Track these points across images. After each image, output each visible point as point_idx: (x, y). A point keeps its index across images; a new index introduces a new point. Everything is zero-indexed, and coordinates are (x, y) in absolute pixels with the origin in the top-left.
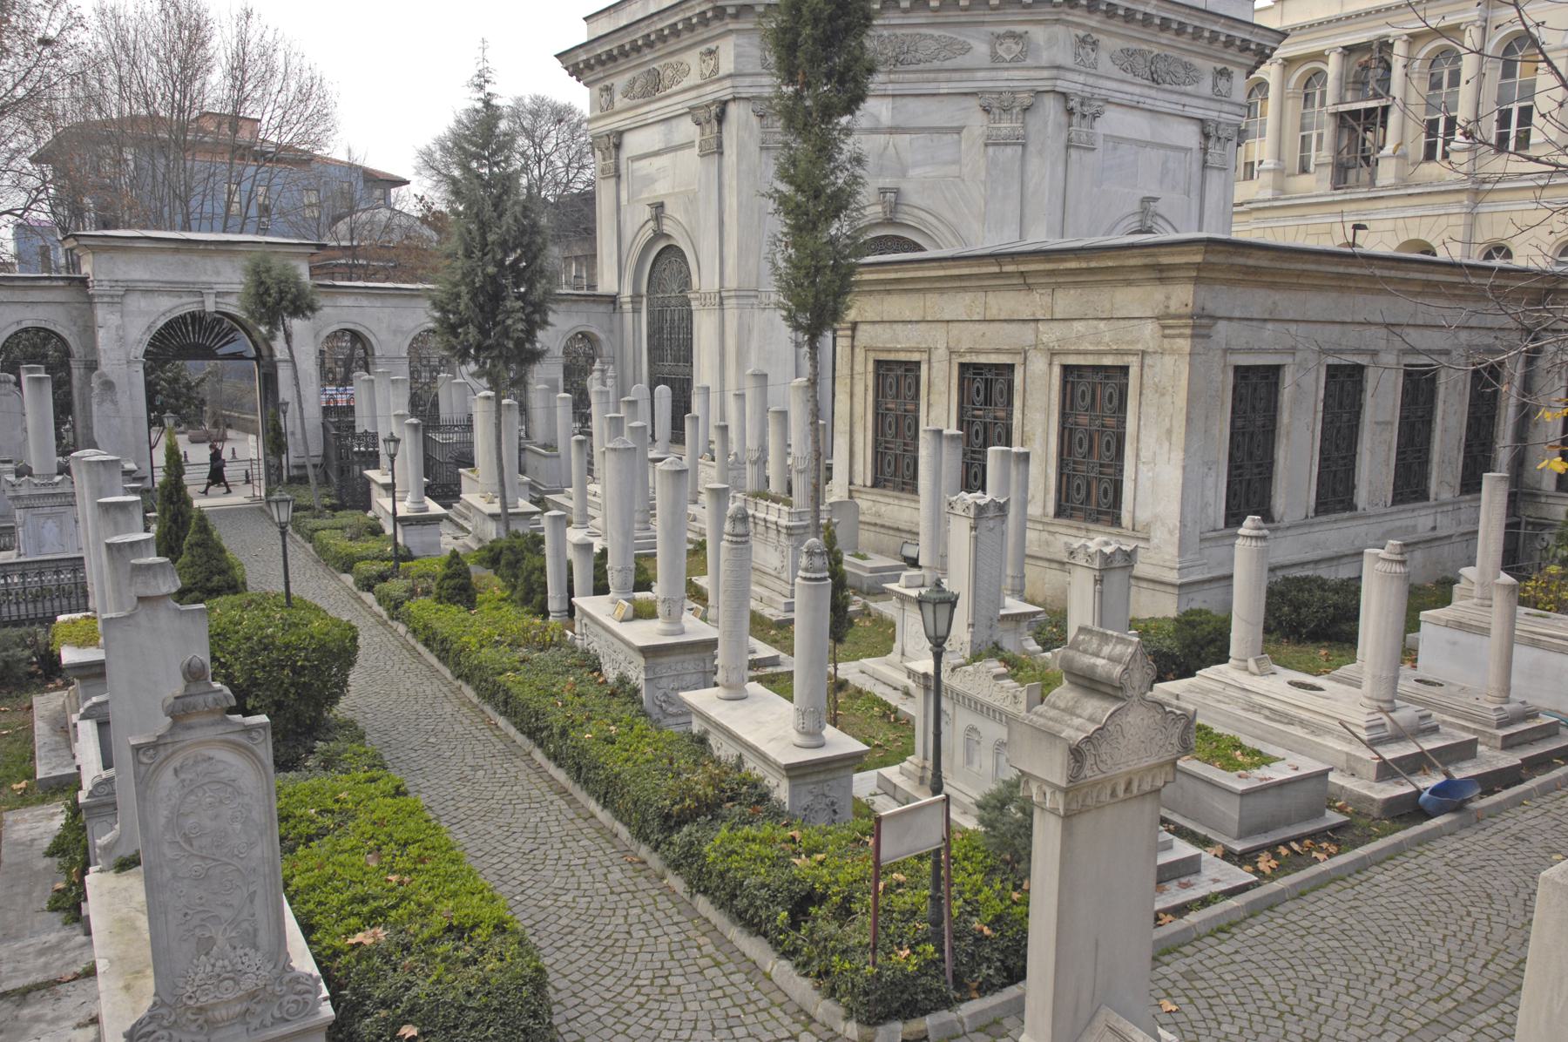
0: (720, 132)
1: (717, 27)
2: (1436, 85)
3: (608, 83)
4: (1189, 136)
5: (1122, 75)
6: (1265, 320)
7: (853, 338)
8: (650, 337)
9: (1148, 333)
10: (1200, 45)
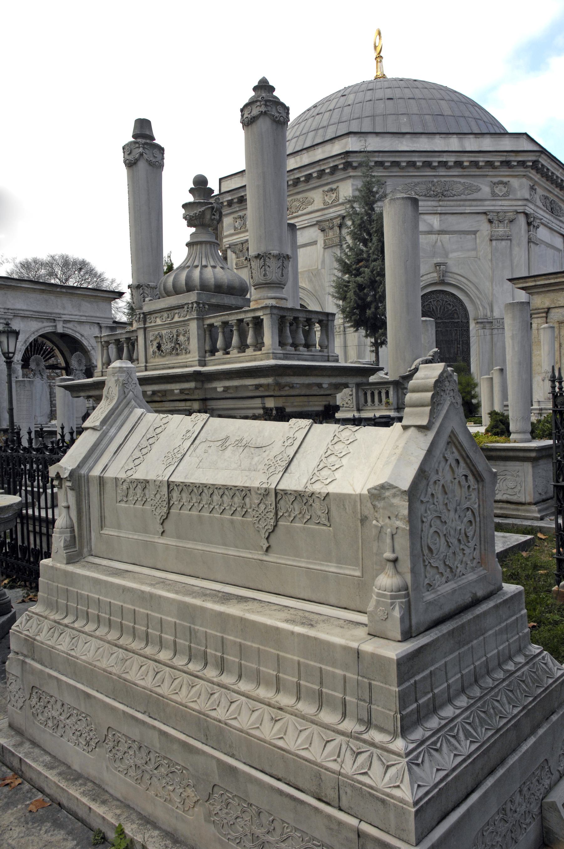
7: (547, 317)
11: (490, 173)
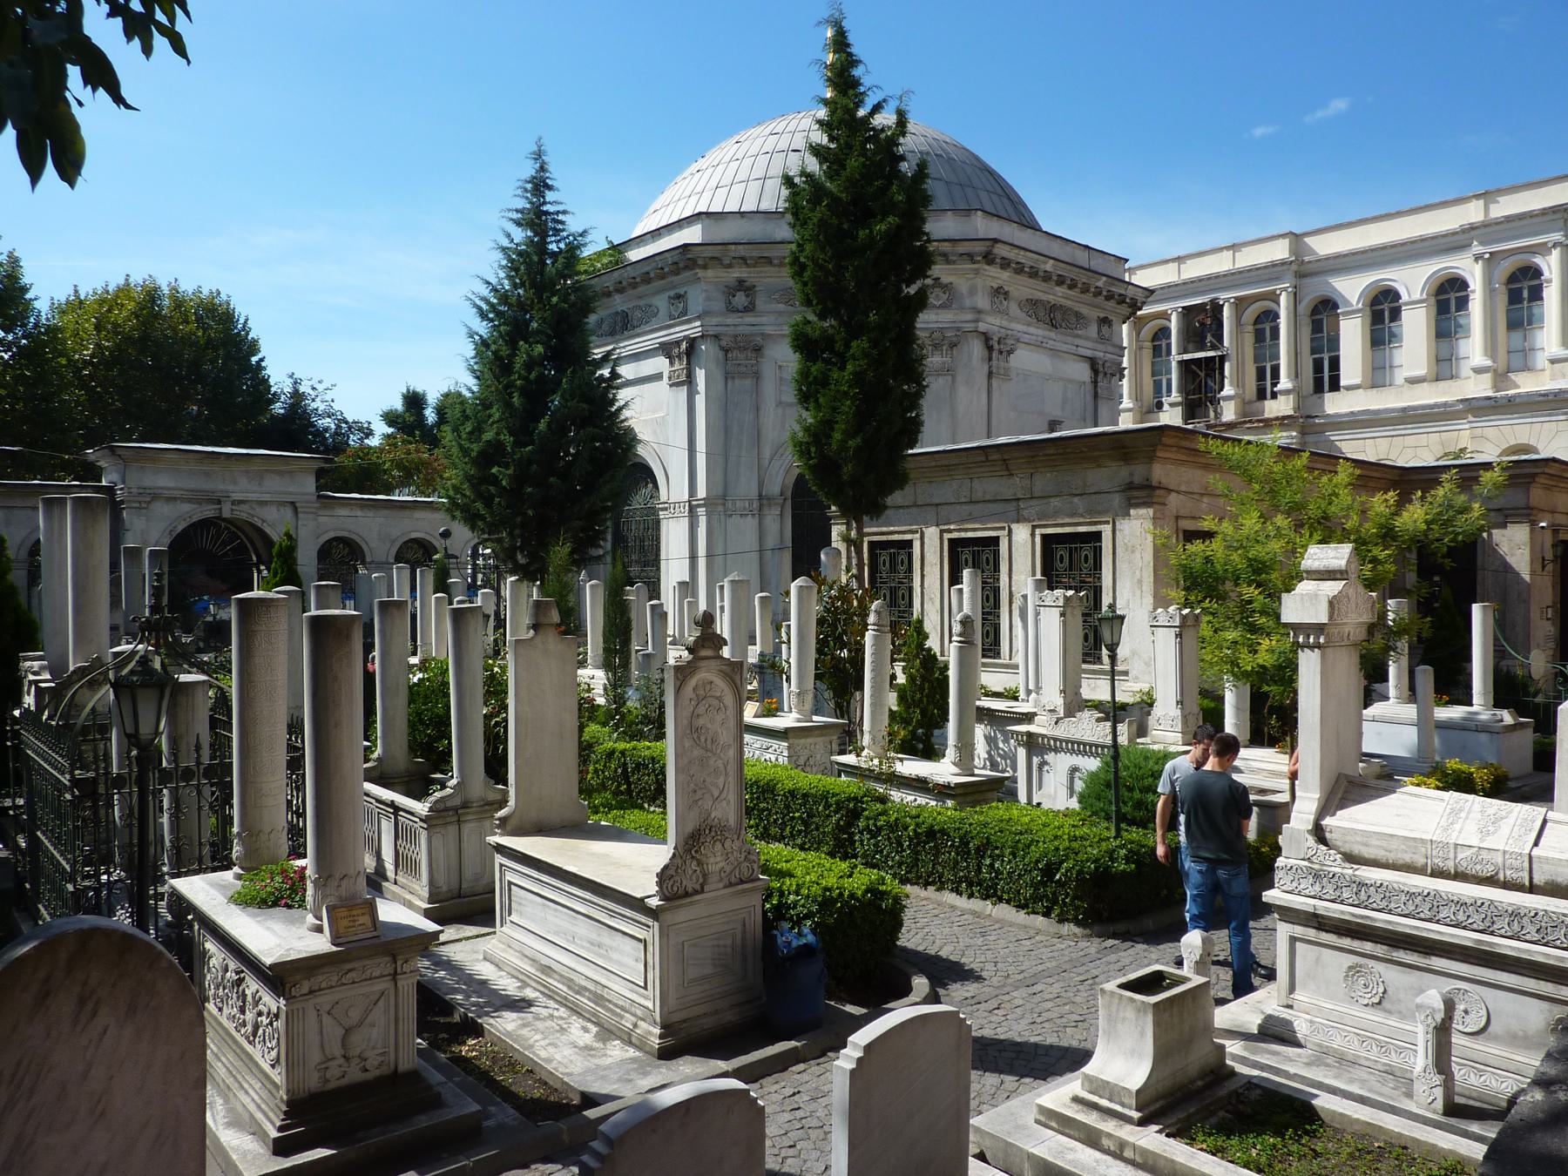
4: (1082, 372)
10: (1088, 297)
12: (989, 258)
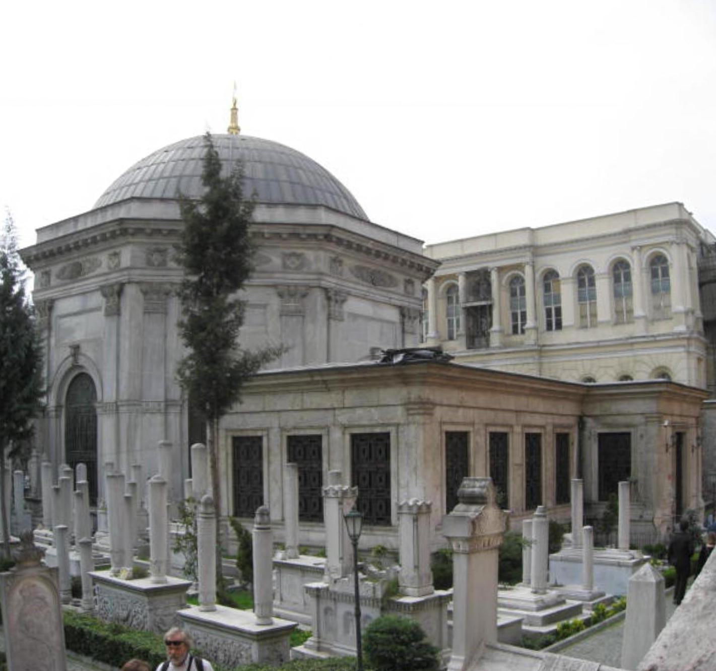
0: (119, 303)
1: (121, 240)
2: (513, 294)
3: (47, 269)
4: (393, 315)
5: (355, 279)
6: (458, 407)
8: (67, 434)
9: (399, 414)
11: (280, 245)
12: (328, 237)
